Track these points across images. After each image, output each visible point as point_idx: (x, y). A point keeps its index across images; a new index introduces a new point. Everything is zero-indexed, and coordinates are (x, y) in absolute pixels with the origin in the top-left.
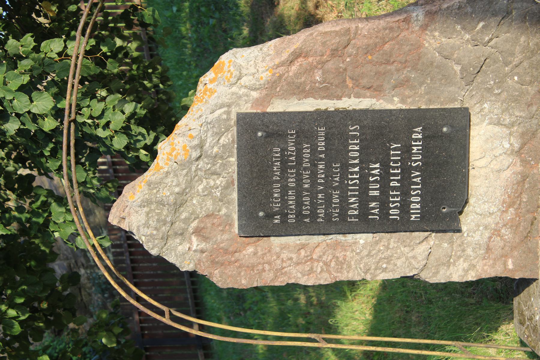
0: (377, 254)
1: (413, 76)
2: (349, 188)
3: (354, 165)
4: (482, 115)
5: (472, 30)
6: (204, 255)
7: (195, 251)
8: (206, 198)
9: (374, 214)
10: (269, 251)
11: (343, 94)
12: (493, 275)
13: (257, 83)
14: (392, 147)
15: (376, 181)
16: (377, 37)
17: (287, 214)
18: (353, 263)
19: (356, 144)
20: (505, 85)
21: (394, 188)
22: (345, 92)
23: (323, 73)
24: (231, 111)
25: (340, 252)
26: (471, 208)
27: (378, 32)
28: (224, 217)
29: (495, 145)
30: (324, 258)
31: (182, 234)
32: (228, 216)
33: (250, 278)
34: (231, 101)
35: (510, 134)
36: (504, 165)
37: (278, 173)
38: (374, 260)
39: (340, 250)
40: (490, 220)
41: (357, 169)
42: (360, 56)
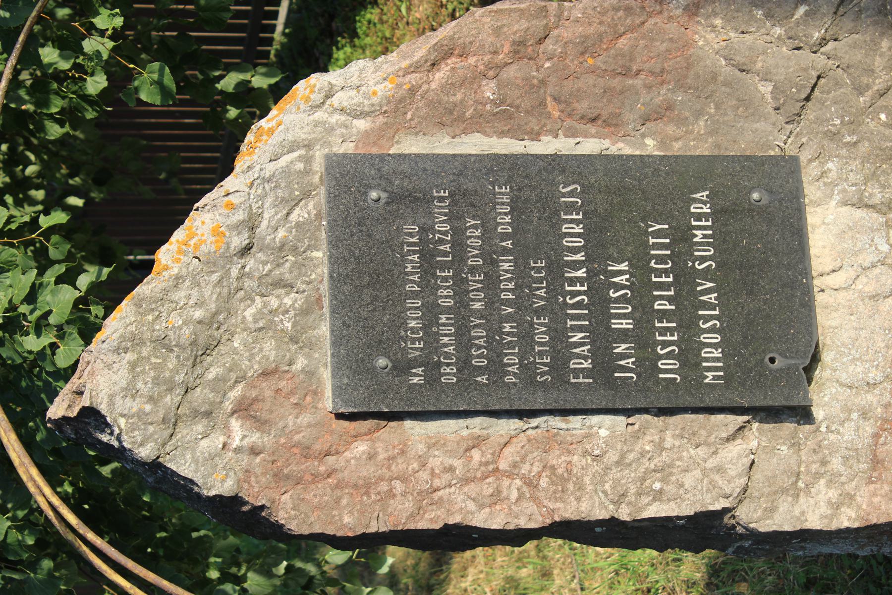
0: (637, 460)
1: (680, 98)
2: (569, 311)
3: (576, 266)
4: (825, 184)
5: (786, 18)
6: (258, 459)
7: (238, 450)
10: (403, 452)
11: (542, 128)
13: (366, 102)
14: (650, 230)
16: (601, 23)
17: (439, 364)
18: (587, 480)
19: (577, 222)
20: (863, 128)
21: (663, 315)
22: (545, 125)
23: (498, 85)
24: (312, 156)
25: (559, 456)
26: (829, 371)
27: (603, 13)
28: (302, 376)
29: (859, 244)
30: (525, 469)
31: (208, 414)
32: (310, 373)
33: (362, 512)
34: (312, 136)
36: (884, 285)
38: (633, 475)
39: (558, 452)
40: (870, 398)
41: (581, 273)
42: (571, 58)
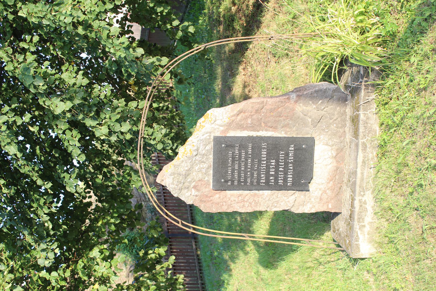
3: (264, 161)
7: (193, 196)
9: (272, 182)
17: (234, 181)
19: (265, 151)
21: (281, 171)
30: (250, 201)
31: (188, 188)
32: (208, 181)
35: (332, 149)
41: (265, 162)
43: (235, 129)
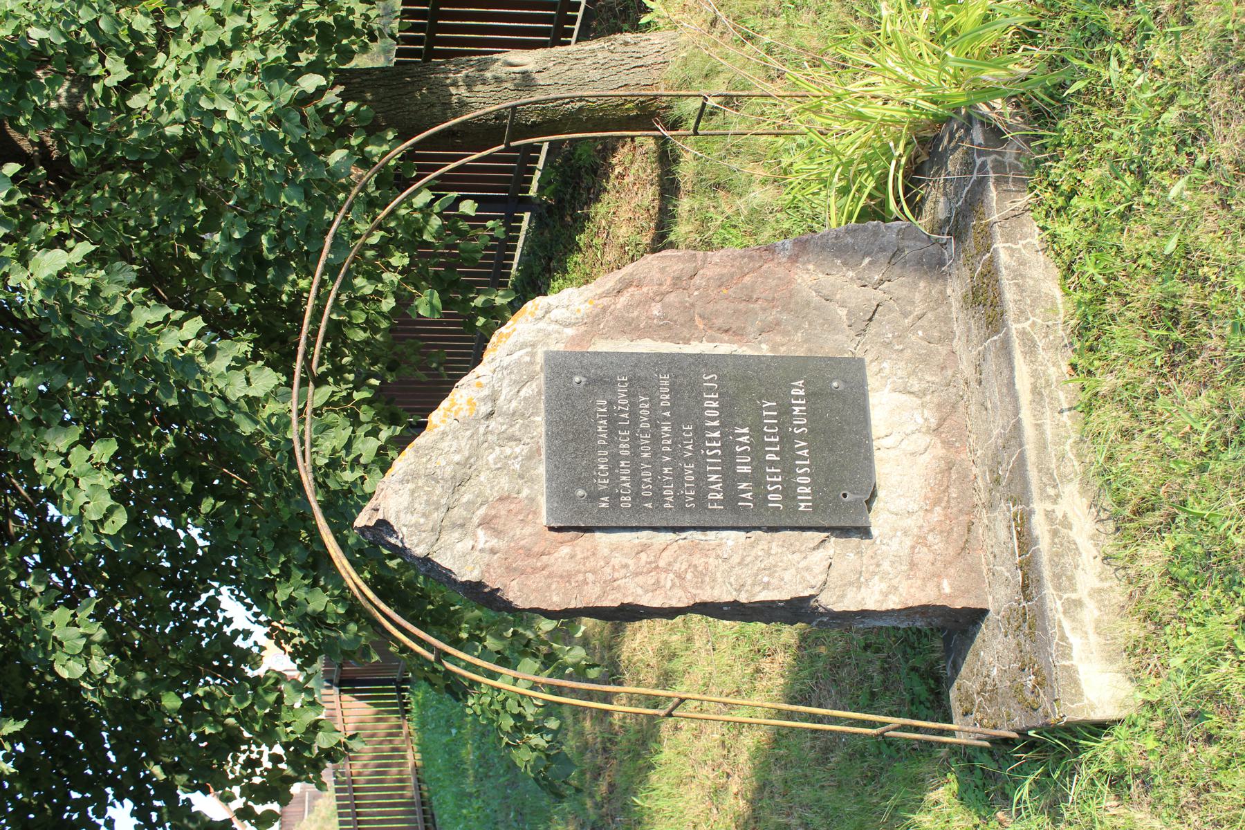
3: (713, 429)
6: (496, 557)
7: (482, 551)
8: (499, 473)
9: (745, 500)
10: (594, 554)
12: (924, 602)
15: (745, 452)
17: (619, 495)
18: (718, 575)
21: (772, 464)
30: (676, 567)
31: (462, 526)
32: (532, 500)
35: (923, 405)
37: (604, 436)
40: (910, 522)
41: (717, 434)
43: (607, 337)
